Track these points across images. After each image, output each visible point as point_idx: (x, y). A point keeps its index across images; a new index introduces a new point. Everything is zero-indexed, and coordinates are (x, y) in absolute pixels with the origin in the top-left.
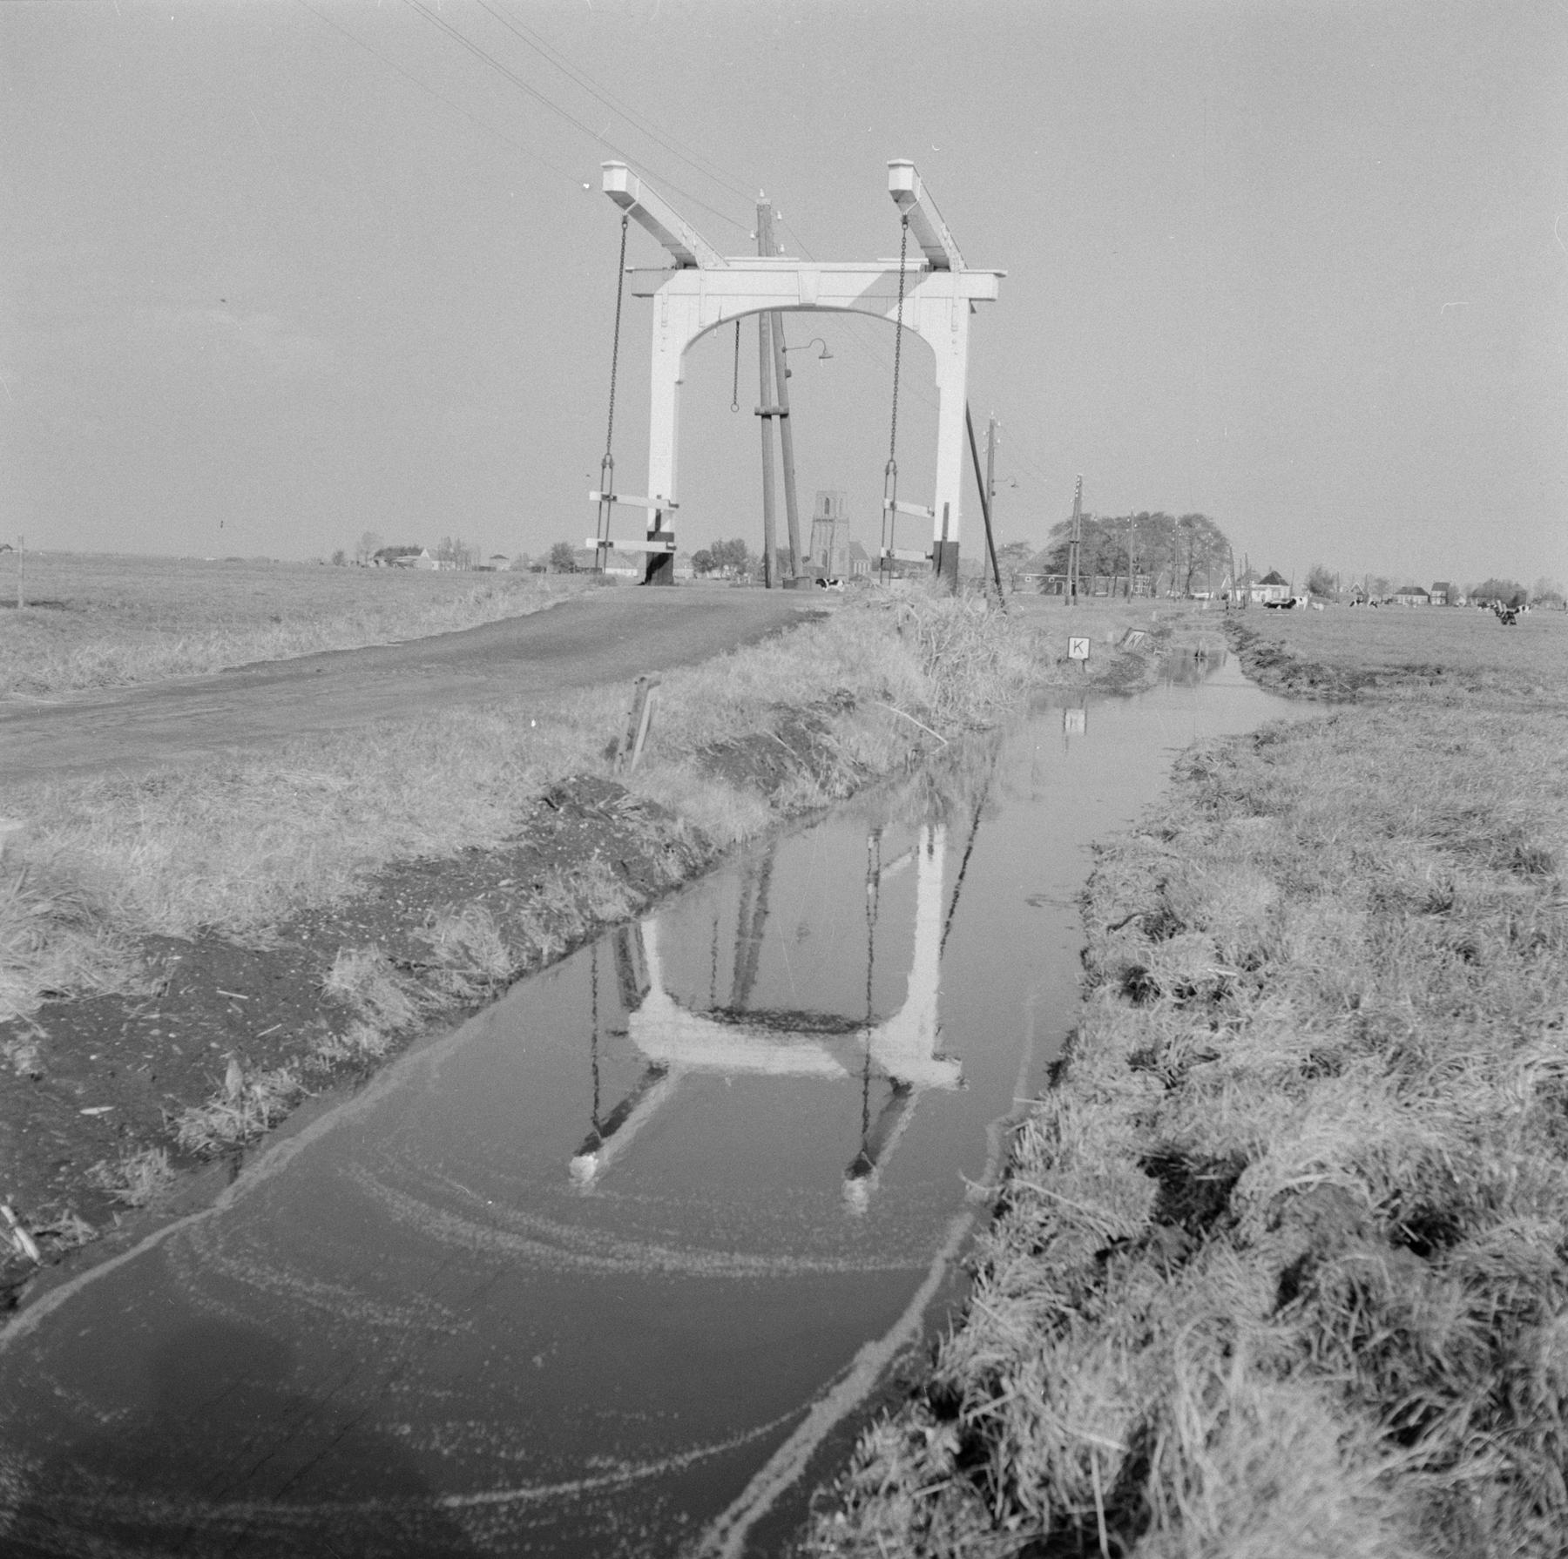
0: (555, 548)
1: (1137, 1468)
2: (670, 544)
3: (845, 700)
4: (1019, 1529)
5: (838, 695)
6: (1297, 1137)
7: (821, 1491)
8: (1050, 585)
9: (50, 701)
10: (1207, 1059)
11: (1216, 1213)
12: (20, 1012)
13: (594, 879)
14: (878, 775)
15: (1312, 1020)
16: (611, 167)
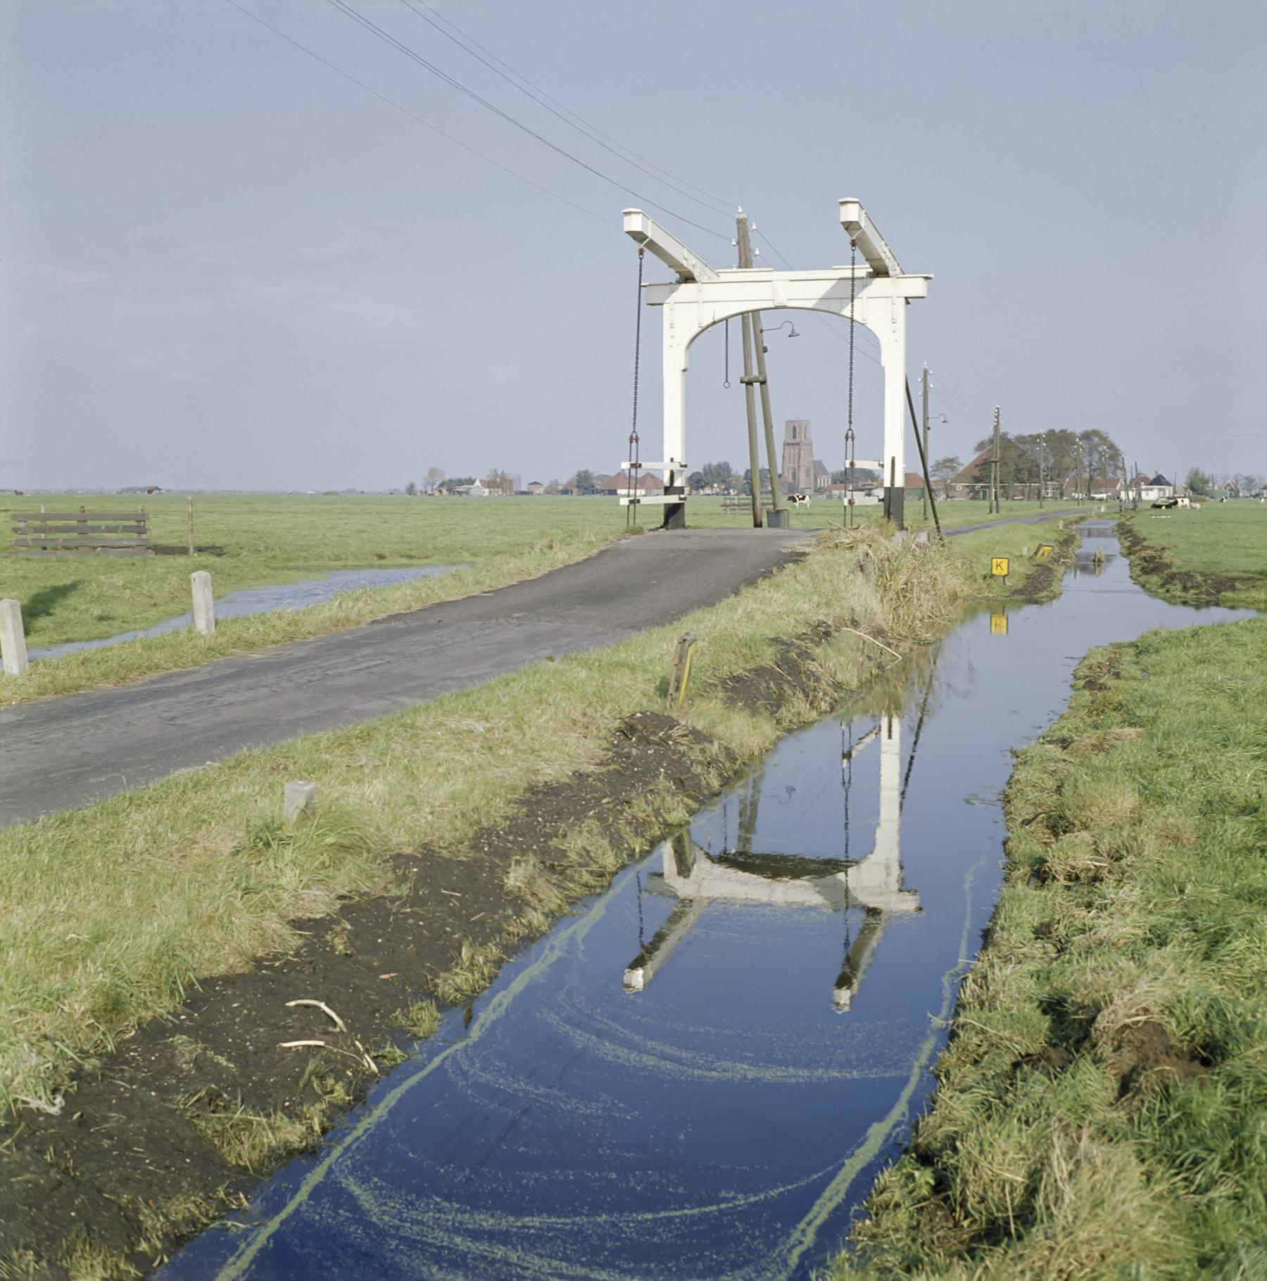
0: (579, 475)
1: (1032, 1191)
2: (682, 496)
3: (823, 630)
4: (969, 1226)
5: (819, 626)
6: (1131, 992)
7: (856, 1207)
8: (978, 492)
9: (257, 656)
10: (1083, 931)
11: (1084, 1038)
12: (328, 911)
13: (664, 794)
14: (851, 691)
15: (1154, 901)
16: (630, 213)
